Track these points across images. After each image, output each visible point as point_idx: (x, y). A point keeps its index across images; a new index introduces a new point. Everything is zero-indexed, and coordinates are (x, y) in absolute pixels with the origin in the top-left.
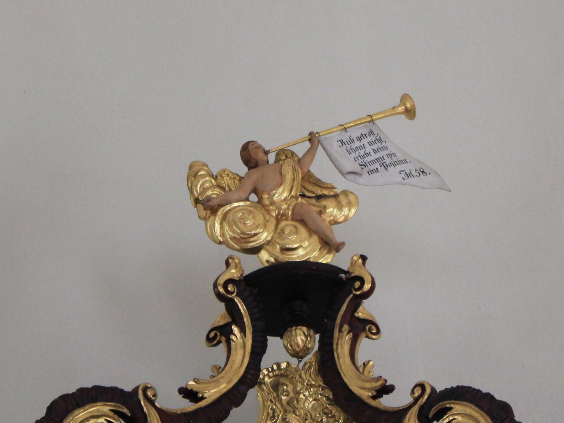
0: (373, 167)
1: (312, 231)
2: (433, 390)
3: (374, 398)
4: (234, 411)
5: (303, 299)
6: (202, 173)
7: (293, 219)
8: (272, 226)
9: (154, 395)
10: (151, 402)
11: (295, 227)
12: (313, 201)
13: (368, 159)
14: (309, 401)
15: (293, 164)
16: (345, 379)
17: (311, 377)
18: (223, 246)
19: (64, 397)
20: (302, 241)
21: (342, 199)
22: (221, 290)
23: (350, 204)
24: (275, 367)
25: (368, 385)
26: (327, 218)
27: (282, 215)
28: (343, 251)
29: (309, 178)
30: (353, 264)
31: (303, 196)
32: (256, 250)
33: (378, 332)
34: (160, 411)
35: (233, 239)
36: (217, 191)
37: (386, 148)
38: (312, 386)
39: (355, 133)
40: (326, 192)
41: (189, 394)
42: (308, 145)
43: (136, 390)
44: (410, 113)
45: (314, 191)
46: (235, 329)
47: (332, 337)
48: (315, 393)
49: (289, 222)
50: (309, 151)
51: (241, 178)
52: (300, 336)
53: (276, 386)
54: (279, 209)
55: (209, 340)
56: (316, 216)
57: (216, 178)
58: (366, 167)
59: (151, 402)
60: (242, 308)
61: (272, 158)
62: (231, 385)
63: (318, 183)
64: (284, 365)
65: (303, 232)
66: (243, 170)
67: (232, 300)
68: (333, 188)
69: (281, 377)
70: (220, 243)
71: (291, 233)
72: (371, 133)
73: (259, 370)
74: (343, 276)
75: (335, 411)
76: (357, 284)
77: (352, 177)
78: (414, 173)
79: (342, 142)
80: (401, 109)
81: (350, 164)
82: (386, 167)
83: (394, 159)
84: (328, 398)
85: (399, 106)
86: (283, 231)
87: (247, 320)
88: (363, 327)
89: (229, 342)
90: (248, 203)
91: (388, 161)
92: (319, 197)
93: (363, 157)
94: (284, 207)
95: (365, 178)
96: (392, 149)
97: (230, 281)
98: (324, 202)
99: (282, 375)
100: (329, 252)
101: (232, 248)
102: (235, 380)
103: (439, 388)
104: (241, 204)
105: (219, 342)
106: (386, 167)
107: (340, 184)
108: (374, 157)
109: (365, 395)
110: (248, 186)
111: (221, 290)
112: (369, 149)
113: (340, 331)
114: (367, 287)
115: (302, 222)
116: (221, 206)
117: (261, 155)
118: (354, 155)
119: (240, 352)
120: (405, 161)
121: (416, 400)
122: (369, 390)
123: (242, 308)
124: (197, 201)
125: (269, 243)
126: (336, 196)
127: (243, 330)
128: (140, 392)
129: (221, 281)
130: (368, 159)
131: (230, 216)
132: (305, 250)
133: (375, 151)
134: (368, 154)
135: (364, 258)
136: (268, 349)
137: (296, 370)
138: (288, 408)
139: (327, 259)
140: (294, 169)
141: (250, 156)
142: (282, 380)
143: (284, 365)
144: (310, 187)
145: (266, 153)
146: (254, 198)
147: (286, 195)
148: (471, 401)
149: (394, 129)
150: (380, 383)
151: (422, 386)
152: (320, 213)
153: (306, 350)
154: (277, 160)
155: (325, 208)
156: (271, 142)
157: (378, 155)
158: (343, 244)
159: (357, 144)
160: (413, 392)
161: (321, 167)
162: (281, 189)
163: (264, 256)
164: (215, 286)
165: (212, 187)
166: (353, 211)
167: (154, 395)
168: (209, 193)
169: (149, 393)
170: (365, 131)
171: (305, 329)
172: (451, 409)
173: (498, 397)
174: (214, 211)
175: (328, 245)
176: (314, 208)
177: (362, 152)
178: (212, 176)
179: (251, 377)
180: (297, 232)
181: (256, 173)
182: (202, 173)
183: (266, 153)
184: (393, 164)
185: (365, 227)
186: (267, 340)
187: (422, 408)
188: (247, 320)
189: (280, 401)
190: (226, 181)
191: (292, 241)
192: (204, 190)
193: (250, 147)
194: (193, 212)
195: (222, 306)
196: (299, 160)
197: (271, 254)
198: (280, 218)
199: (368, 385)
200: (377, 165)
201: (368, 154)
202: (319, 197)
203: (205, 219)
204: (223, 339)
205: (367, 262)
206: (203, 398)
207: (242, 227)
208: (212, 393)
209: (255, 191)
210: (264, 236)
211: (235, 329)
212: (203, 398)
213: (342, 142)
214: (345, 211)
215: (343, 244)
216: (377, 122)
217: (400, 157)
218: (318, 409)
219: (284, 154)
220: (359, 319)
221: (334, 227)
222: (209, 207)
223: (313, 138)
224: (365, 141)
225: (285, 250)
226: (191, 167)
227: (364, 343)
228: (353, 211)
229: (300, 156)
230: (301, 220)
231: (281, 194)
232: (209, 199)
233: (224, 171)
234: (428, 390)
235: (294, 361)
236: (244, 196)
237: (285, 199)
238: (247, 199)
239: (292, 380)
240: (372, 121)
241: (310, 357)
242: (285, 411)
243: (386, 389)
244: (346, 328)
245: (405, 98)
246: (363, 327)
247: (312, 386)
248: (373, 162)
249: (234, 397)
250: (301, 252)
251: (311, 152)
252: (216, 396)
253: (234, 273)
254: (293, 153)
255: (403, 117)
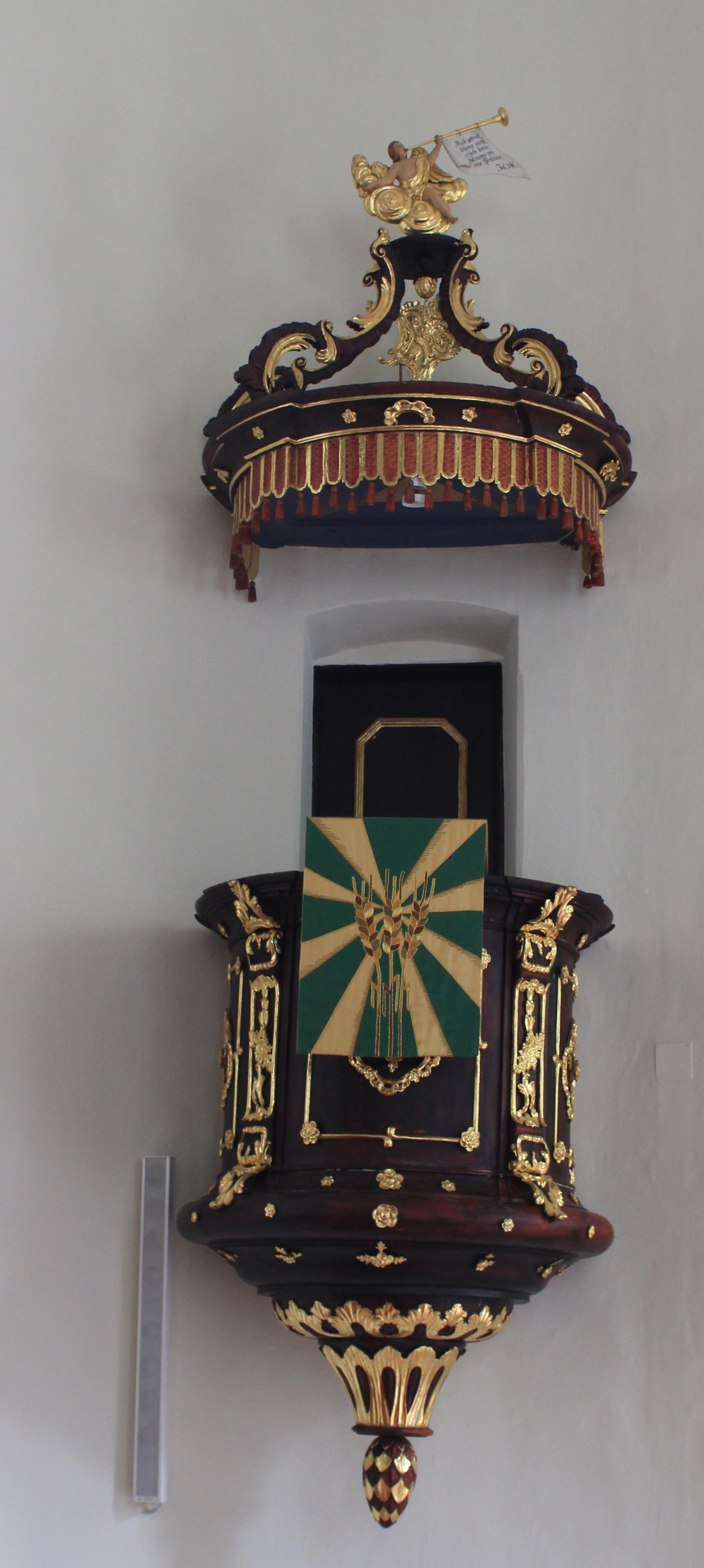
0: (478, 161)
1: (436, 209)
2: (515, 329)
3: (475, 331)
4: (383, 337)
5: (429, 258)
6: (362, 164)
7: (424, 200)
8: (409, 204)
9: (332, 328)
10: (329, 332)
11: (425, 205)
12: (437, 186)
13: (475, 156)
14: (431, 329)
15: (423, 159)
16: (457, 316)
17: (433, 312)
18: (376, 218)
19: (273, 331)
20: (429, 216)
21: (457, 184)
22: (375, 252)
23: (462, 189)
24: (410, 305)
25: (472, 322)
26: (446, 199)
27: (416, 196)
28: (456, 224)
29: (435, 169)
30: (463, 235)
31: (430, 181)
32: (398, 222)
33: (478, 279)
34: (335, 339)
35: (383, 213)
36: (372, 178)
37: (487, 148)
38: (434, 319)
39: (466, 136)
40: (446, 180)
41: (355, 326)
42: (434, 145)
43: (319, 324)
44: (505, 121)
45: (439, 180)
46: (384, 280)
47: (448, 286)
48: (436, 323)
49: (420, 202)
50: (435, 149)
51: (389, 168)
52: (427, 283)
53: (410, 318)
54: (414, 192)
55: (366, 282)
56: (438, 197)
57: (371, 168)
58: (474, 162)
59: (329, 332)
60: (389, 265)
61: (409, 154)
62: (381, 319)
63: (440, 173)
64: (415, 304)
65: (430, 209)
66: (389, 162)
67: (382, 259)
68: (450, 177)
69: (414, 312)
70: (374, 215)
71: (421, 211)
72: (478, 136)
73: (399, 307)
74: (456, 243)
75: (449, 336)
76: (466, 250)
77: (464, 169)
78: (506, 166)
79: (458, 143)
80: (498, 119)
81: (463, 160)
82: (487, 161)
83: (493, 156)
84: (444, 328)
85: (497, 116)
86: (416, 208)
87: (392, 273)
88: (467, 276)
89: (379, 288)
90: (393, 187)
91: (488, 157)
92: (441, 183)
93: (471, 154)
94: (418, 191)
95: (473, 170)
96: (492, 149)
97: (381, 246)
98: (444, 187)
99: (414, 310)
100: (447, 223)
101: (381, 219)
102: (384, 315)
103: (519, 329)
104: (388, 188)
105: (372, 284)
106: (487, 161)
107: (455, 173)
108: (479, 154)
109: (470, 329)
110: (393, 174)
111: (375, 252)
112: (476, 148)
113: (454, 282)
114: (473, 252)
115: (429, 201)
116: (375, 189)
117: (402, 153)
118: (465, 152)
119: (387, 296)
120: (500, 158)
121: (504, 335)
122: (472, 326)
123: (389, 265)
124: (358, 186)
125: (406, 216)
126: (452, 183)
127: (389, 280)
128: (322, 325)
129: (376, 245)
130: (475, 156)
131: (381, 197)
132: (432, 224)
133: (480, 150)
134: (475, 152)
135: (471, 231)
136: (406, 293)
137: (424, 307)
138: (418, 333)
139: (444, 229)
140: (425, 164)
141: (395, 152)
142: (414, 314)
143: (415, 304)
144: (436, 177)
145: (406, 150)
146: (397, 183)
147: (418, 181)
148: (539, 340)
149: (493, 133)
150: (479, 322)
151: (508, 326)
152: (442, 195)
153: (431, 294)
154: (413, 155)
155: (445, 191)
156: (409, 143)
157: (482, 153)
158: (457, 219)
159: (467, 144)
160: (502, 330)
161: (443, 162)
162: (415, 178)
163: (403, 225)
164: (371, 249)
165: (368, 175)
166: (464, 192)
167: (332, 328)
168: (367, 179)
169: (328, 326)
170: (473, 135)
171: (430, 279)
172: (526, 344)
173: (557, 337)
174: (370, 192)
175: (447, 218)
176: (437, 192)
177: (471, 150)
178: (368, 166)
179: (394, 314)
180: (426, 209)
181: (399, 165)
182: (362, 164)
183: (406, 150)
184: (492, 159)
185: (472, 210)
186: (404, 284)
187: (507, 341)
188: (392, 273)
189: (413, 328)
190: (378, 170)
191: (423, 215)
192: (363, 177)
193: (395, 146)
194: (355, 192)
195: (375, 262)
196: (428, 156)
197: (408, 225)
198: (415, 198)
199: (472, 322)
200: (481, 160)
201: (475, 152)
202: (441, 183)
203: (364, 197)
204: (375, 282)
205: (474, 234)
206: (362, 329)
207: (388, 204)
208: (368, 325)
209: (398, 178)
210: (404, 212)
211: (384, 280)
212: (362, 329)
213: (458, 143)
214: (459, 193)
215: (457, 219)
216: (482, 128)
217: (497, 154)
218: (438, 335)
219: (418, 151)
220: (465, 270)
221: (450, 205)
222: (366, 189)
223: (438, 140)
224: (473, 142)
225: (417, 222)
226: (354, 159)
227: (469, 286)
228: (464, 192)
229: (429, 152)
230: (428, 200)
231: (416, 181)
232: (366, 184)
233: (377, 163)
234: (511, 331)
235: (422, 300)
236: (390, 182)
237: (418, 185)
238: (392, 184)
239: (421, 314)
240: (478, 128)
241: (433, 298)
242: (416, 336)
243: (485, 326)
244: (458, 281)
245: (501, 110)
246: (467, 276)
247: (434, 319)
248: (478, 158)
249: (383, 327)
250: (428, 223)
251: (436, 150)
252: (371, 327)
253: (384, 240)
254: (424, 150)
255: (500, 124)
